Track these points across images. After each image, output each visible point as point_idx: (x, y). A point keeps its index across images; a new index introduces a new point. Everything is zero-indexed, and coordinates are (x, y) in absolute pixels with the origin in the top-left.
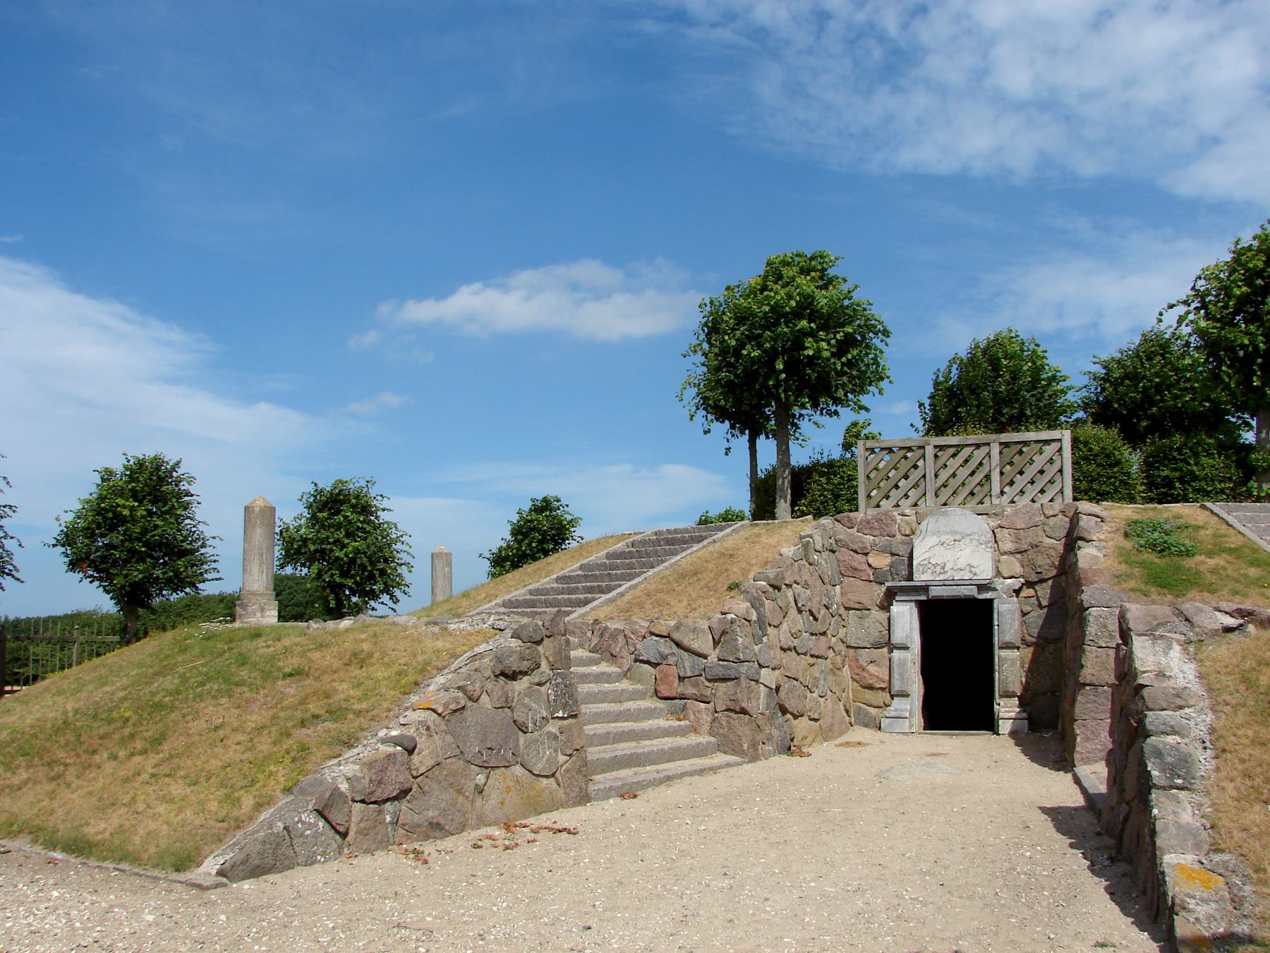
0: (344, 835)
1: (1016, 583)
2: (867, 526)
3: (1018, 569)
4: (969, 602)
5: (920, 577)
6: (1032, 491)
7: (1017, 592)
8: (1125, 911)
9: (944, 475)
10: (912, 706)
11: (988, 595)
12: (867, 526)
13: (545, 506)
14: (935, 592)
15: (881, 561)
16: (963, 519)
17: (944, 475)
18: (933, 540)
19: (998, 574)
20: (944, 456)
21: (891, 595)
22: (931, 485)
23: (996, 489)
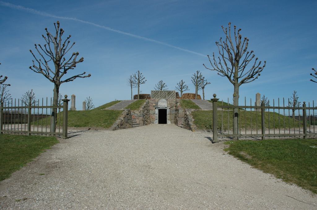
0: (219, 57)
1: (170, 107)
2: (152, 100)
3: (169, 106)
4: (159, 111)
5: (159, 107)
6: (171, 97)
7: (170, 108)
8: (266, 171)
9: (161, 95)
10: (157, 121)
11: (166, 109)
12: (152, 100)
13: (5, 77)
14: (160, 108)
15: (154, 104)
16: (164, 100)
17: (161, 95)
18: (161, 102)
19: (167, 106)
20: (161, 93)
21: (155, 108)
22: (159, 96)
23: (167, 97)
